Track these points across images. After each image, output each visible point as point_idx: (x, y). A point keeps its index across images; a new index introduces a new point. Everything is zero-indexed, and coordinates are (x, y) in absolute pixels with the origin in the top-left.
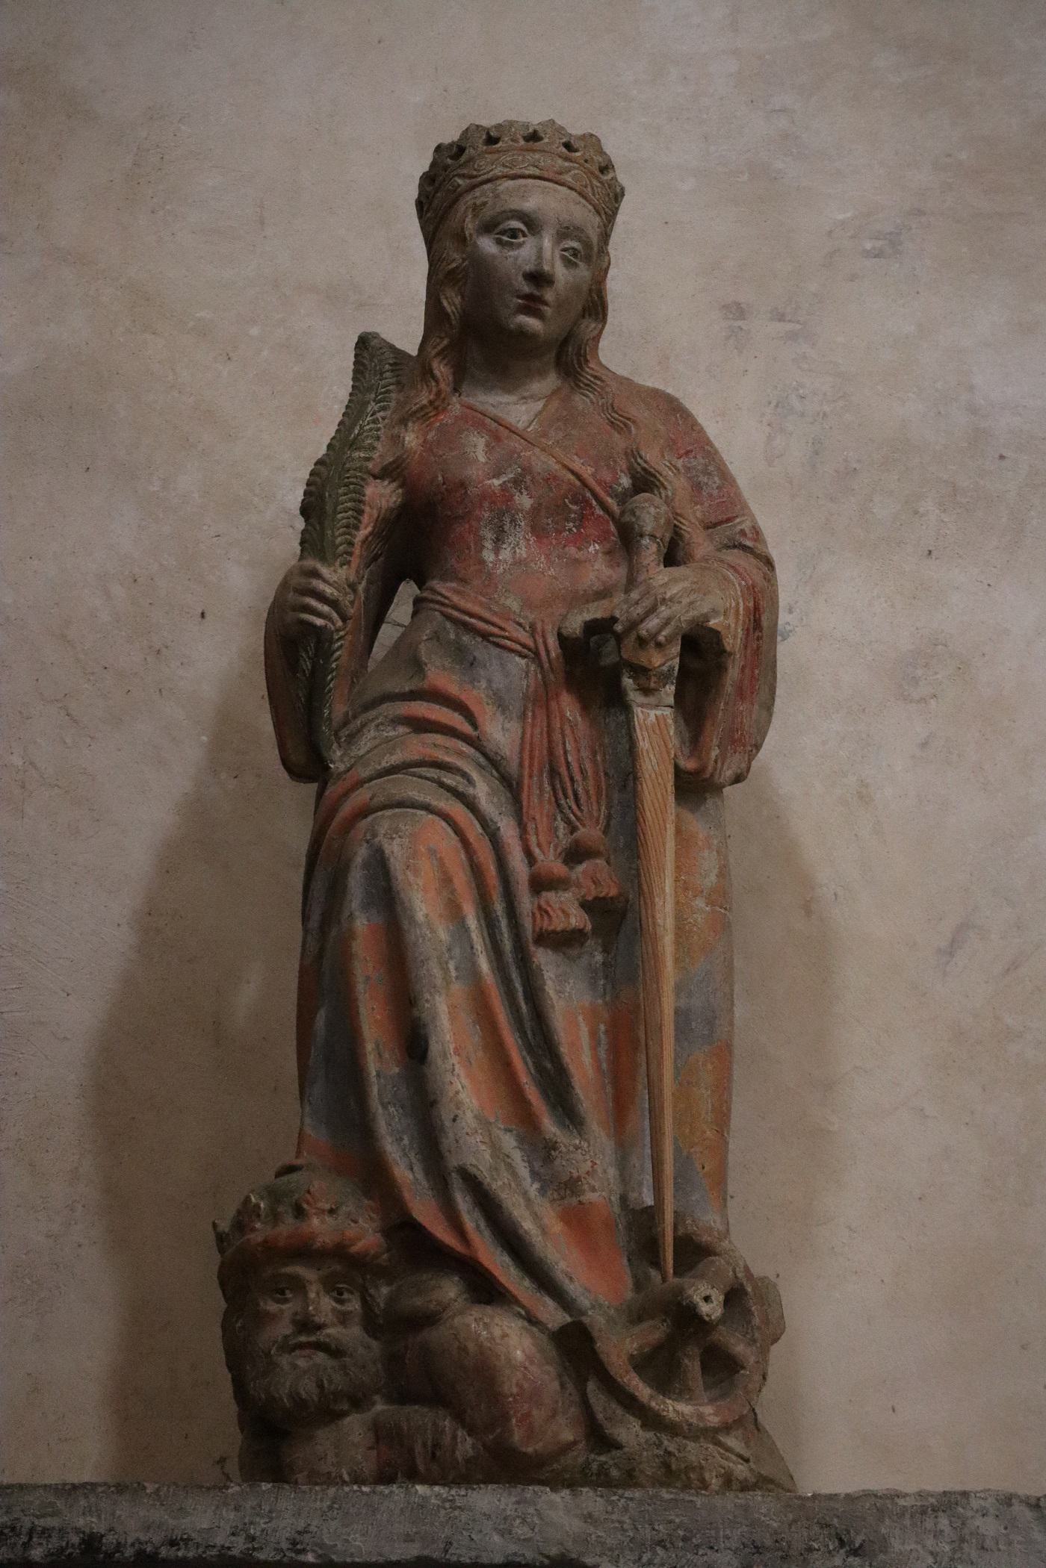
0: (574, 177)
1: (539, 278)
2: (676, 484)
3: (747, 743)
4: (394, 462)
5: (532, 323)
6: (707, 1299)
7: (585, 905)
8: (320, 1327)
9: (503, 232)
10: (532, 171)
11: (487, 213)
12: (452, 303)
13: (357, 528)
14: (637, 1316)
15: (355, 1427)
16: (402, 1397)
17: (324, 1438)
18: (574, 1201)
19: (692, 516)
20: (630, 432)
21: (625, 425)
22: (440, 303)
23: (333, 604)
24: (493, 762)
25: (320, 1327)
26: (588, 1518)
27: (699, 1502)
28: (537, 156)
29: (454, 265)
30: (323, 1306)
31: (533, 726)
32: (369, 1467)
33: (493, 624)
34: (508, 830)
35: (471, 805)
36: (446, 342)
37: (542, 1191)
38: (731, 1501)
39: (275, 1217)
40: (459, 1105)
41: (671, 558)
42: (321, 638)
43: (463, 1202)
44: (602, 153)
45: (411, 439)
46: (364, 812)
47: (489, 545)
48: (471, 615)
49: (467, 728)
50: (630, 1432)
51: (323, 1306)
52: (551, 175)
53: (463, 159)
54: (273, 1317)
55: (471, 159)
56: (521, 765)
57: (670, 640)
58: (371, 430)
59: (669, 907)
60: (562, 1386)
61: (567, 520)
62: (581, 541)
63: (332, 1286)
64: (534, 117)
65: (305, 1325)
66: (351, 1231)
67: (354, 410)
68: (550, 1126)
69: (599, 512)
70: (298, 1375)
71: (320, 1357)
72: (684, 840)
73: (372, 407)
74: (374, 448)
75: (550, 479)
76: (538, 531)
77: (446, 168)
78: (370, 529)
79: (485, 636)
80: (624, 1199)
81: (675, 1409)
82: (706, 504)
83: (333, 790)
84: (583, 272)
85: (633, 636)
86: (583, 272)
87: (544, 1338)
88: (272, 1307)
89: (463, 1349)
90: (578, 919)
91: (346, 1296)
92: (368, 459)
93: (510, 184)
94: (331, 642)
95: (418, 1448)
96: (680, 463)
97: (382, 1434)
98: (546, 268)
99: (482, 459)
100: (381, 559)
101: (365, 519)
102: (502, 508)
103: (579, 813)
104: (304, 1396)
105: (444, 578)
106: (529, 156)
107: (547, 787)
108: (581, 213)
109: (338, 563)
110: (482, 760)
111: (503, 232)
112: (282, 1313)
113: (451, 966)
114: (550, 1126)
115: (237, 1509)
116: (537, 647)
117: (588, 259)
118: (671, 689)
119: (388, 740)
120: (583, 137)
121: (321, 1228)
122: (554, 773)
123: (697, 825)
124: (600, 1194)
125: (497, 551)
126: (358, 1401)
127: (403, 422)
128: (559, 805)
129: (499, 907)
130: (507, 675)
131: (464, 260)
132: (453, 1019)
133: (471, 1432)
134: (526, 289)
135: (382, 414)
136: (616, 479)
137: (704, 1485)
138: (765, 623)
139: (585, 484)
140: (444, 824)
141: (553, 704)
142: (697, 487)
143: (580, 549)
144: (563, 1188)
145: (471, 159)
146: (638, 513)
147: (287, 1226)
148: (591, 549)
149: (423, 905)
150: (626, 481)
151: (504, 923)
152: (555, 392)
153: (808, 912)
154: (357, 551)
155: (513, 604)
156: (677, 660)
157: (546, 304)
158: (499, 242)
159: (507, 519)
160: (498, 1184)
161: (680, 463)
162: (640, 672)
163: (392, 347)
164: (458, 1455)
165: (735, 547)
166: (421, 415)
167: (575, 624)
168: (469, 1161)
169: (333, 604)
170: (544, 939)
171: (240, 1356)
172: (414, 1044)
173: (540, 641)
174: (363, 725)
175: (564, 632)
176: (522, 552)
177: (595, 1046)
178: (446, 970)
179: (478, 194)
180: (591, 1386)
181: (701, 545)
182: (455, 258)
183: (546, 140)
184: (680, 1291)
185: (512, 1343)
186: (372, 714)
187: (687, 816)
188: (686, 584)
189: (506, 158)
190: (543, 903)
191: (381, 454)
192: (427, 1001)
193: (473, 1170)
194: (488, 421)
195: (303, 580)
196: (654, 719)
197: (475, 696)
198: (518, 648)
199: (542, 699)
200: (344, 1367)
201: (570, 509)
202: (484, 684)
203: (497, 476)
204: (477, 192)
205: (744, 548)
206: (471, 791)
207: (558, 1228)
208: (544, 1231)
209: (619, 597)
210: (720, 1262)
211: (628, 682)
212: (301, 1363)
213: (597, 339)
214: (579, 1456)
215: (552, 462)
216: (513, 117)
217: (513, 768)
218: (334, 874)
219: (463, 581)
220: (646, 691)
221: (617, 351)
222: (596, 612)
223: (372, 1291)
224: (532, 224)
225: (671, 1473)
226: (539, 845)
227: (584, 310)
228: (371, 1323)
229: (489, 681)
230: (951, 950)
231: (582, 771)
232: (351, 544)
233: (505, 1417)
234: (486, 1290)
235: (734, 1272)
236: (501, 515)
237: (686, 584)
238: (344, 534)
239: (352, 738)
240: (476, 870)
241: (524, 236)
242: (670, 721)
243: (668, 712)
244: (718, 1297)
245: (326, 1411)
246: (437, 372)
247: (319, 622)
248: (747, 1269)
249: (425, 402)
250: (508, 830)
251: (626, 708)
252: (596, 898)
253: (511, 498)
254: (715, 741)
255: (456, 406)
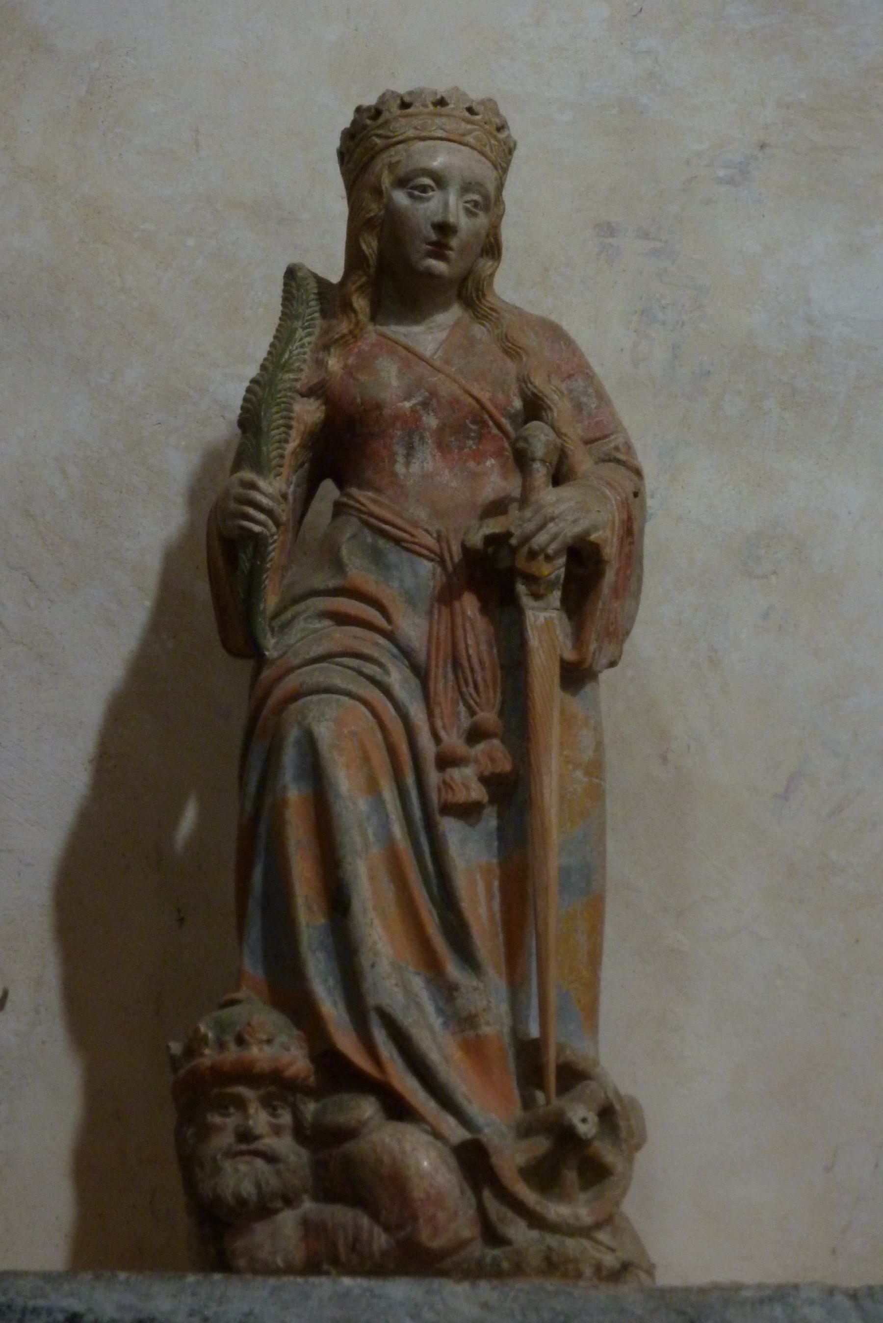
0: (475, 138)
1: (444, 229)
2: (560, 407)
3: (617, 634)
4: (319, 383)
5: (438, 266)
6: (582, 1118)
7: (484, 780)
8: (257, 1138)
9: (415, 188)
10: (440, 133)
11: (402, 171)
12: (370, 245)
13: (286, 441)
14: (525, 1131)
15: (287, 1221)
16: (327, 1193)
17: (261, 1232)
18: (471, 1034)
19: (574, 432)
20: (521, 359)
21: (517, 353)
22: (360, 246)
23: (269, 512)
24: (406, 653)
25: (257, 1138)
26: (485, 1306)
27: (577, 1292)
28: (444, 120)
29: (372, 214)
30: (260, 1119)
31: (439, 623)
32: (298, 1256)
33: (405, 531)
34: (417, 712)
35: (387, 691)
36: (364, 279)
37: (445, 1024)
38: (604, 1292)
39: (221, 1045)
40: (376, 953)
41: (558, 479)
42: (258, 542)
43: (380, 1036)
44: (497, 114)
45: (334, 363)
46: (295, 696)
47: (401, 459)
48: (386, 522)
49: (381, 622)
50: (519, 1232)
51: (260, 1119)
52: (457, 138)
53: (381, 120)
54: (219, 1129)
55: (387, 122)
56: (429, 656)
57: (557, 553)
58: (299, 354)
59: (554, 784)
60: (463, 1192)
61: (468, 438)
62: (479, 456)
63: (268, 1103)
64: (441, 87)
65: (245, 1136)
66: (285, 1058)
67: (283, 338)
68: (453, 970)
69: (495, 431)
70: (240, 1178)
71: (259, 1163)
72: (568, 721)
73: (300, 333)
74: (301, 370)
75: (454, 403)
76: (442, 446)
77: (365, 127)
78: (297, 442)
79: (397, 541)
80: (514, 1031)
81: (557, 1211)
82: (586, 423)
83: (267, 674)
84: (482, 220)
85: (525, 550)
86: (482, 220)
87: (447, 1151)
88: (217, 1119)
89: (380, 1161)
90: (477, 792)
91: (280, 1111)
92: (296, 380)
93: (420, 145)
94: (266, 545)
95: (341, 1241)
96: (563, 386)
97: (311, 1229)
98: (452, 220)
99: (395, 383)
100: (306, 465)
101: (293, 433)
102: (412, 426)
103: (478, 700)
104: (245, 1195)
105: (360, 487)
106: (438, 121)
107: (450, 675)
108: (484, 171)
109: (272, 476)
110: (395, 651)
111: (415, 188)
112: (227, 1123)
113: (370, 831)
114: (453, 970)
115: (194, 1294)
116: (442, 553)
117: (487, 209)
118: (557, 594)
119: (315, 631)
120: (482, 102)
121: (260, 1055)
122: (456, 664)
123: (576, 704)
124: (496, 1022)
125: (407, 464)
126: (289, 1201)
127: (326, 348)
128: (461, 693)
129: (410, 780)
130: (416, 575)
131: (380, 210)
132: (372, 878)
133: (386, 1228)
134: (434, 237)
135: (308, 339)
136: (510, 403)
137: (579, 1275)
138: (636, 527)
139: (483, 407)
140: (363, 709)
141: (457, 604)
142: (579, 407)
143: (479, 464)
144: (463, 1022)
145: (387, 122)
146: (531, 440)
147: (232, 1053)
148: (488, 463)
149: (345, 780)
150: (518, 404)
151: (414, 794)
152: (457, 323)
153: (664, 759)
154: (287, 461)
155: (421, 514)
156: (563, 569)
157: (451, 249)
158: (411, 196)
159: (416, 439)
160: (408, 1020)
161: (563, 386)
162: (531, 579)
163: (315, 276)
164: (375, 1247)
165: (610, 461)
166: (343, 342)
167: (476, 539)
168: (385, 1001)
169: (269, 512)
170: (448, 809)
171: (189, 1163)
172: (337, 900)
173: (445, 547)
174: (294, 618)
175: (469, 544)
176: (429, 466)
177: (490, 897)
178: (364, 835)
179: (393, 153)
180: (487, 1194)
181: (583, 461)
182: (374, 209)
183: (452, 106)
184: (561, 1114)
185: (424, 1159)
186: (301, 606)
187: (568, 697)
188: (572, 504)
189: (415, 122)
190: (448, 779)
191: (306, 376)
192: (350, 864)
193: (388, 1010)
194: (400, 349)
195: (241, 491)
196: (544, 621)
197: (388, 593)
198: (426, 552)
199: (447, 596)
200: (278, 1173)
201: (468, 427)
202: (396, 584)
203: (408, 397)
204: (392, 151)
205: (618, 461)
206: (385, 679)
207: (457, 1054)
208: (447, 1060)
209: (514, 511)
210: (593, 1085)
211: (521, 588)
212: (243, 1168)
213: (492, 275)
214: (478, 1250)
215: (454, 387)
216: (422, 85)
217: (422, 657)
218: (263, 732)
219: (378, 490)
220: (537, 596)
221: (511, 284)
222: (493, 527)
223: (302, 1107)
224: (440, 181)
225: (553, 1265)
226: (444, 727)
227: (482, 251)
228: (300, 1133)
229: (402, 581)
230: (785, 796)
231: (481, 662)
232: (282, 456)
233: (414, 1218)
234: (398, 1109)
235: (605, 1093)
236: (410, 435)
237: (572, 504)
238: (277, 448)
239: (286, 626)
240: (391, 750)
241: (433, 190)
242: (557, 622)
243: (554, 614)
244: (593, 1118)
245: (264, 1209)
246: (356, 305)
247: (257, 528)
248: (616, 1092)
249: (345, 331)
250: (417, 712)
251: (520, 611)
252: (493, 774)
253: (419, 419)
254: (593, 636)
255: (372, 333)
